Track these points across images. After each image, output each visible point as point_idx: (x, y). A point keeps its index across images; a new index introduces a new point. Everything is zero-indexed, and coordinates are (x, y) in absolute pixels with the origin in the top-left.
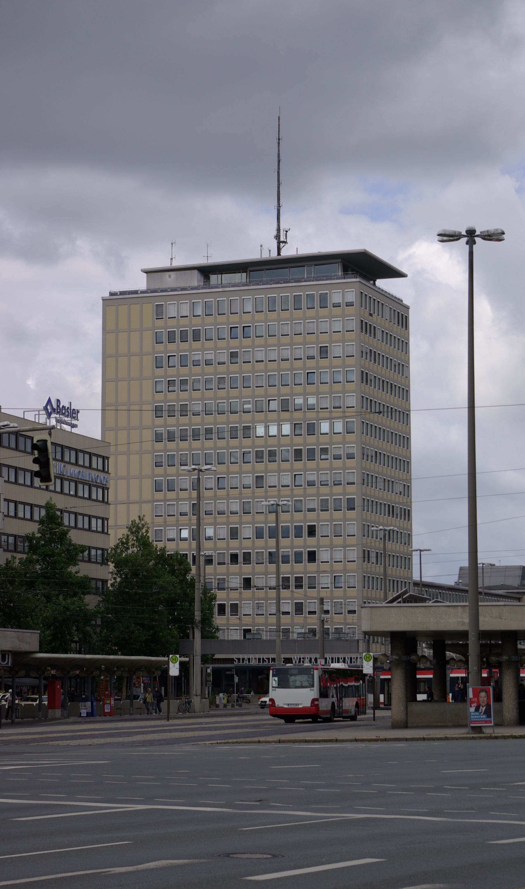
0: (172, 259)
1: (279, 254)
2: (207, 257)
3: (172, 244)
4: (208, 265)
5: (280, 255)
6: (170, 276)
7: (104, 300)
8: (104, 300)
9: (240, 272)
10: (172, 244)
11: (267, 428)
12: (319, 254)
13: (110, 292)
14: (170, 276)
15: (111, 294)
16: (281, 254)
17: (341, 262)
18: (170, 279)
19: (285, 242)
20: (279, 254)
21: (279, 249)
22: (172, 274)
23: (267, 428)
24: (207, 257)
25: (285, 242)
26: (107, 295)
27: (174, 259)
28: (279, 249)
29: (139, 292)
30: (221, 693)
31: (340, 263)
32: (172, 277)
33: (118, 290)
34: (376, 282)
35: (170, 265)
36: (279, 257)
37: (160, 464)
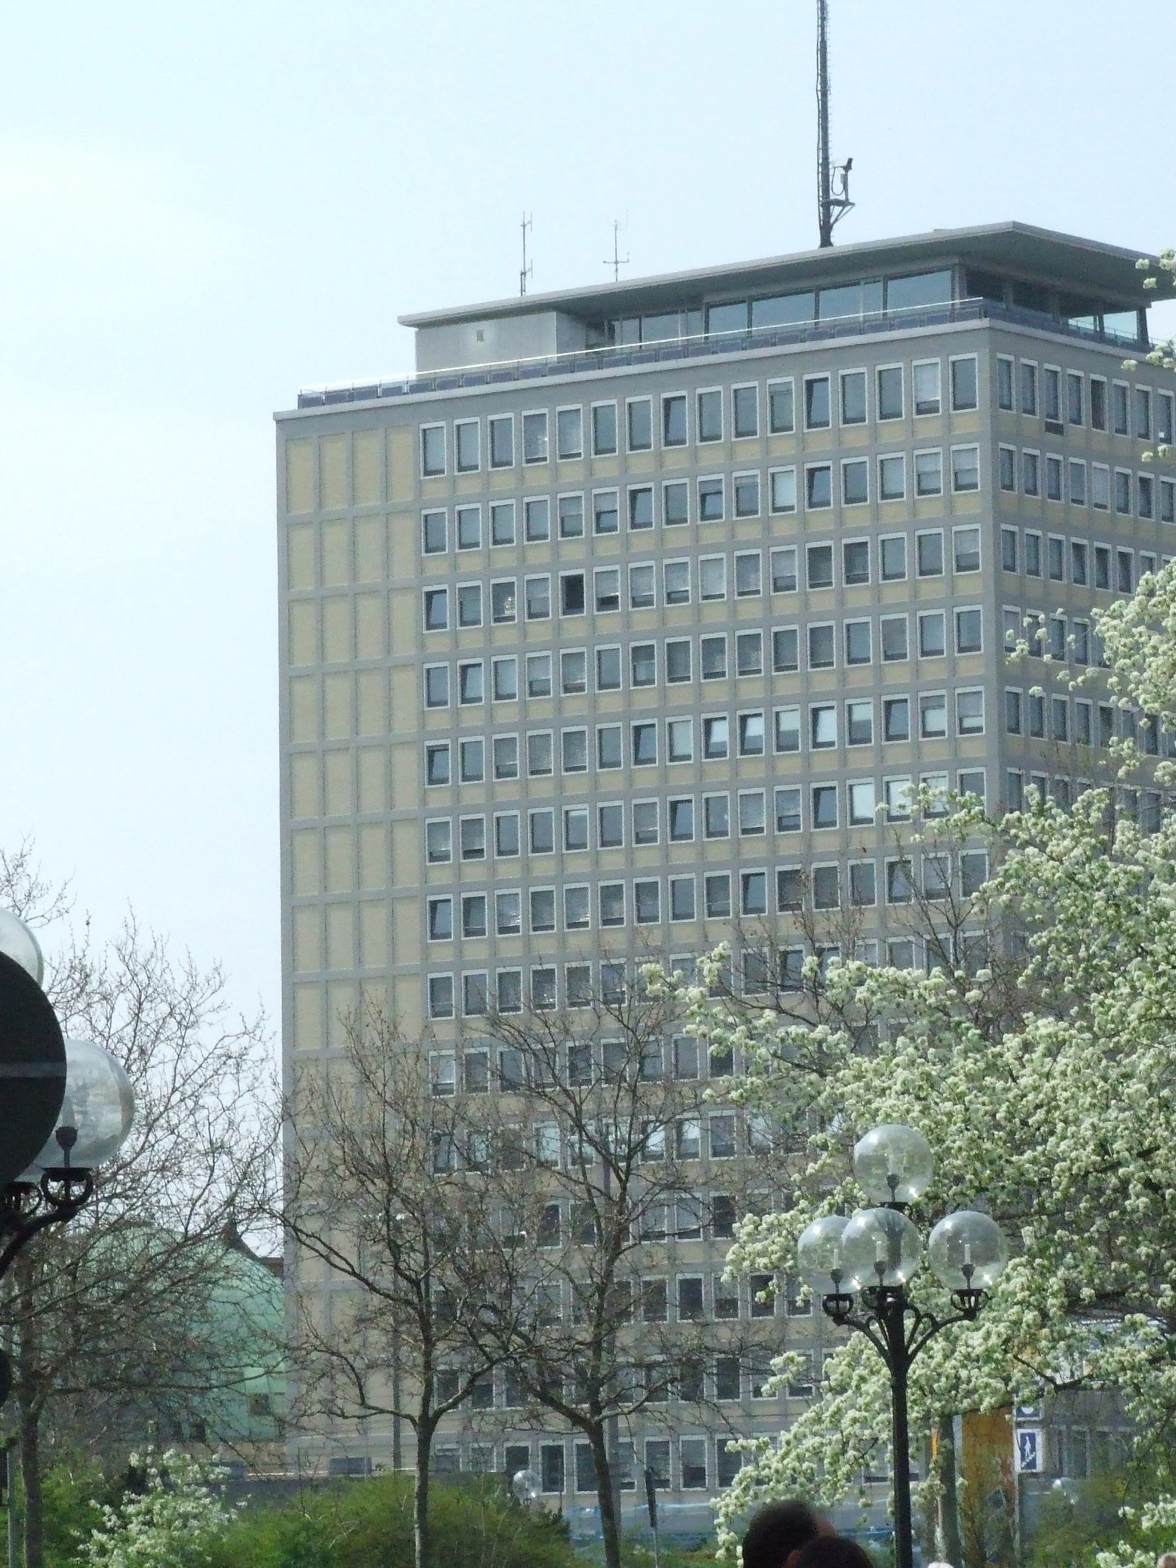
0: (523, 274)
1: (826, 241)
2: (616, 263)
3: (524, 226)
4: (617, 288)
5: (831, 244)
6: (480, 337)
7: (282, 422)
8: (282, 422)
9: (683, 311)
10: (524, 226)
11: (884, 793)
12: (938, 236)
13: (300, 396)
14: (480, 337)
15: (305, 401)
16: (832, 240)
17: (960, 264)
18: (481, 344)
19: (843, 204)
20: (826, 241)
21: (826, 228)
22: (487, 326)
23: (884, 793)
24: (616, 263)
25: (843, 204)
26: (290, 405)
27: (528, 274)
28: (826, 228)
29: (406, 389)
30: (910, 1548)
31: (957, 268)
32: (485, 336)
33: (323, 390)
34: (1148, 311)
35: (519, 295)
36: (827, 251)
37: (791, 822)
